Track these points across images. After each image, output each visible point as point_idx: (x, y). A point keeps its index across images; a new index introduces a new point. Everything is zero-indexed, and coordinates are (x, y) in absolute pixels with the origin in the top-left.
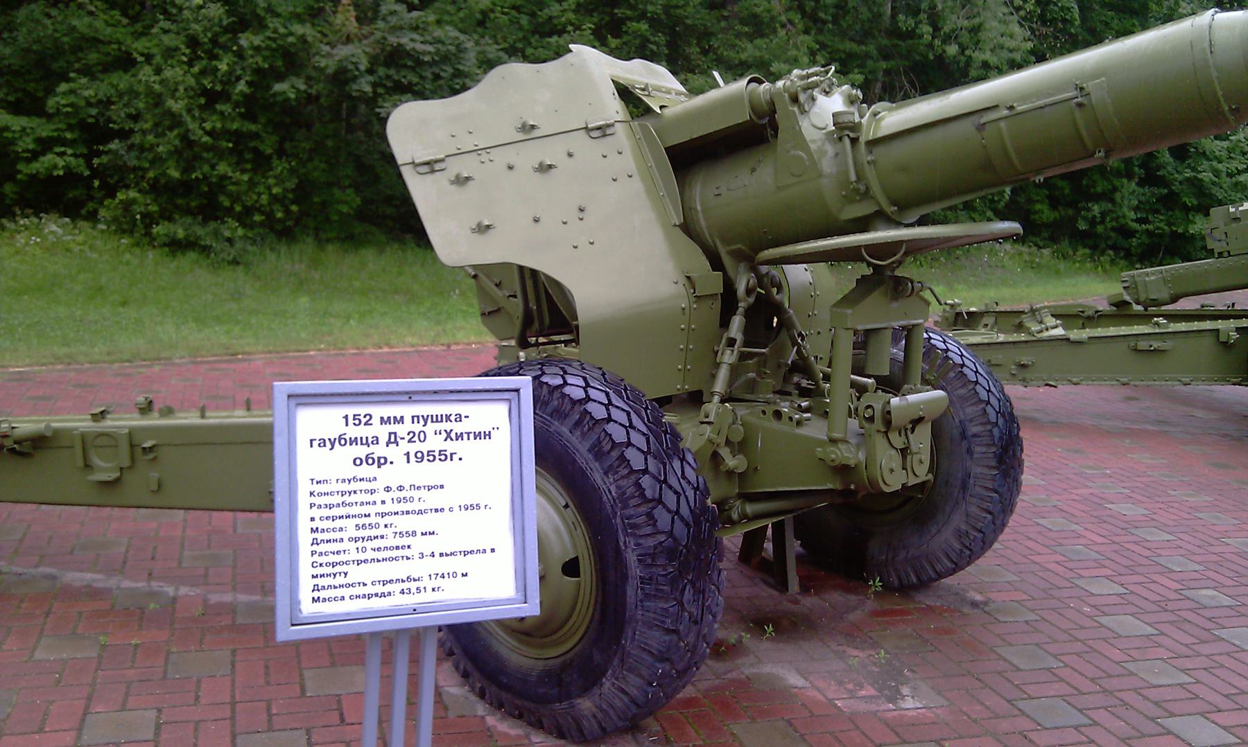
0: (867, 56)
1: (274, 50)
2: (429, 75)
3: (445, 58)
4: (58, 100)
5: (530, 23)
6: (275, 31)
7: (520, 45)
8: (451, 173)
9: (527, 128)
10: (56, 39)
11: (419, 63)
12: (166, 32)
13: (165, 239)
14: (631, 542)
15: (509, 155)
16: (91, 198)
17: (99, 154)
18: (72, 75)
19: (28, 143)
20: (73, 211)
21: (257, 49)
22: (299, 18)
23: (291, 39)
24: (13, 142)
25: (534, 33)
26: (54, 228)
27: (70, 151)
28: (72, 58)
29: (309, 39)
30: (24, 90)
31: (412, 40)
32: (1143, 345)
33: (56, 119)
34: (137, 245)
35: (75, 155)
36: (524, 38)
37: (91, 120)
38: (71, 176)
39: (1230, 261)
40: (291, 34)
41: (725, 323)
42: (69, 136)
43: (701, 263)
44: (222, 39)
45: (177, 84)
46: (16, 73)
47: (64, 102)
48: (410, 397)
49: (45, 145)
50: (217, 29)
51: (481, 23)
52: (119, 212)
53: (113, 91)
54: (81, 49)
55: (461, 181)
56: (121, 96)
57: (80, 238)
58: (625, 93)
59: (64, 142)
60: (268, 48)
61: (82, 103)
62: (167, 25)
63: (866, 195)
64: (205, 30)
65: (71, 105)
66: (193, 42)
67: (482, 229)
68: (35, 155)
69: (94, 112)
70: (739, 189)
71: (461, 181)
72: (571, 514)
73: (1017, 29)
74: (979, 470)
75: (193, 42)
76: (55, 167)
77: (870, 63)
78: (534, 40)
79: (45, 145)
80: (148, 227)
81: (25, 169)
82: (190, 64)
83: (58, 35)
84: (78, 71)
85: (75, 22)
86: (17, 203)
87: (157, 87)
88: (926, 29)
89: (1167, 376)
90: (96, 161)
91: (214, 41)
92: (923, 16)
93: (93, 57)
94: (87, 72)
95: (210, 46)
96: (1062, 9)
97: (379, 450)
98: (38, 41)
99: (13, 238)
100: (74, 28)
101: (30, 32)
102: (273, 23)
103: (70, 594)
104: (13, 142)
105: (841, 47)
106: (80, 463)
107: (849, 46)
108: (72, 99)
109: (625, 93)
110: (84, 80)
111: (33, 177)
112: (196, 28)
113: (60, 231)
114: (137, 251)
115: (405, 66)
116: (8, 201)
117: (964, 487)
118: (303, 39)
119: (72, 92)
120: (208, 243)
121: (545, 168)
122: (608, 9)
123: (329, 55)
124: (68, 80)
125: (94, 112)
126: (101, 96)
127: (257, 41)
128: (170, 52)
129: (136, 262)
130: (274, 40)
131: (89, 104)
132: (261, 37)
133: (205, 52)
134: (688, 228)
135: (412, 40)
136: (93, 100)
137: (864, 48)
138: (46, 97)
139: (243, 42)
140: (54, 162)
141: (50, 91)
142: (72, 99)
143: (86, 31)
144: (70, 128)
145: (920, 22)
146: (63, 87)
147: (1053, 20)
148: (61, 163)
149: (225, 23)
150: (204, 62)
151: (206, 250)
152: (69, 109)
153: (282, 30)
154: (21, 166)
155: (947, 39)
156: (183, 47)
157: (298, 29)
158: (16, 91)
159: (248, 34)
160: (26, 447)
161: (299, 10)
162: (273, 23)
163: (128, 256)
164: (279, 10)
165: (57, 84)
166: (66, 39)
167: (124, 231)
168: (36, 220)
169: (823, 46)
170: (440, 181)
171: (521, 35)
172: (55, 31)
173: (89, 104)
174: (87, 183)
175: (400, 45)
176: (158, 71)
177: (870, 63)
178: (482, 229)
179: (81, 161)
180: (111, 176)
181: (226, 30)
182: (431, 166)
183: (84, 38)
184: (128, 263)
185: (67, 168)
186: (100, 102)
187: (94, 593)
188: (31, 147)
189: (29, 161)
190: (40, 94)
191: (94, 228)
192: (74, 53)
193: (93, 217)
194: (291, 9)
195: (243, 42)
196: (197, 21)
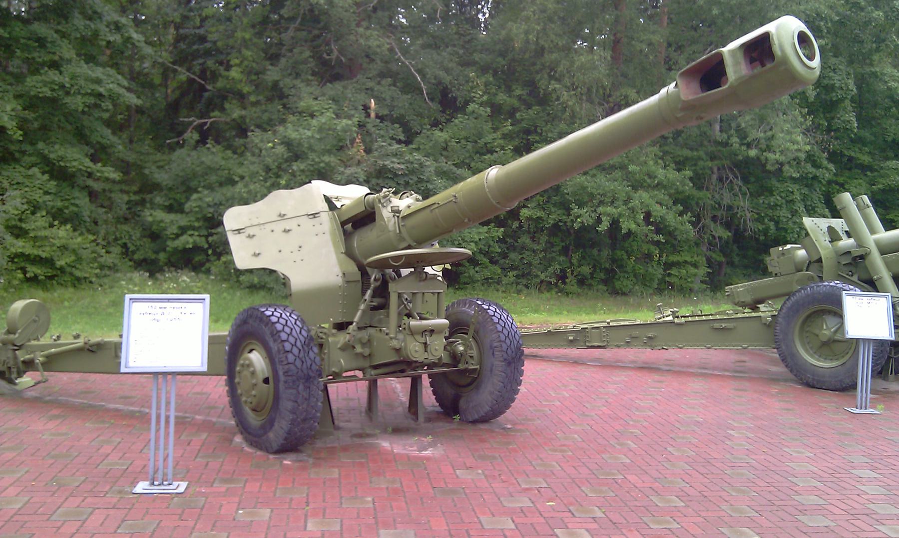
0: (700, 158)
1: (312, 171)
2: (402, 182)
3: (412, 172)
4: (191, 204)
5: (473, 147)
6: (313, 160)
7: (467, 161)
8: (246, 234)
9: (282, 216)
10: (193, 169)
11: (396, 175)
12: (253, 163)
13: (248, 284)
14: (281, 367)
15: (272, 226)
16: (208, 261)
17: (211, 235)
18: (200, 189)
19: (174, 229)
20: (197, 268)
21: (303, 171)
22: (329, 152)
23: (322, 165)
24: (165, 229)
25: (477, 153)
26: (185, 278)
27: (196, 233)
28: (202, 179)
29: (332, 164)
30: (174, 199)
31: (392, 162)
32: (717, 325)
33: (189, 215)
34: (232, 288)
35: (200, 236)
36: (470, 156)
37: (210, 215)
38: (197, 249)
39: (781, 279)
40: (323, 161)
41: (364, 293)
42: (196, 224)
43: (353, 268)
44: (284, 166)
45: (256, 193)
46: (170, 189)
47: (194, 205)
48: (169, 300)
49: (183, 230)
50: (280, 160)
51: (445, 149)
52: (222, 268)
53: (223, 198)
54: (207, 174)
55: (250, 237)
56: (227, 201)
57: (199, 284)
58: (328, 200)
59: (194, 229)
60: (309, 170)
61: (205, 205)
62: (254, 159)
63: (404, 240)
64: (274, 161)
65: (199, 207)
66: (268, 169)
67: (257, 255)
68: (177, 236)
69: (211, 210)
70: (366, 237)
71: (250, 237)
72: (267, 360)
73: (799, 138)
74: (497, 363)
75: (268, 169)
76: (188, 243)
77: (701, 163)
78: (476, 157)
79: (183, 230)
80: (238, 277)
81: (171, 245)
82: (265, 180)
83: (194, 166)
84: (204, 187)
85: (204, 159)
86: (166, 264)
87: (245, 195)
88: (735, 140)
89: (734, 344)
90: (210, 239)
91: (279, 167)
92: (733, 132)
93: (213, 178)
94: (210, 187)
95: (276, 170)
96: (844, 122)
97: (157, 317)
98: (183, 170)
99: (161, 284)
100: (202, 163)
101: (179, 165)
102: (312, 156)
103: (108, 410)
104: (165, 229)
105: (680, 153)
106: (113, 354)
107: (687, 153)
108: (199, 203)
109: (328, 200)
110: (206, 192)
111: (175, 249)
112: (269, 160)
113: (188, 280)
114: (231, 291)
115: (387, 177)
116: (161, 263)
117: (491, 371)
118: (328, 164)
119: (200, 199)
120: (272, 286)
121: (286, 231)
122: (525, 136)
123: (343, 173)
124: (198, 192)
125: (211, 210)
126: (216, 201)
127: (302, 167)
128: (253, 175)
129: (229, 297)
130: (312, 165)
131: (209, 206)
132: (305, 164)
133: (274, 174)
134: (349, 253)
135: (392, 162)
136: (211, 204)
137: (695, 153)
138: (186, 202)
139: (295, 168)
140: (187, 241)
141: (188, 199)
142: (199, 203)
143: (208, 163)
144: (198, 220)
145: (732, 135)
146: (195, 196)
147: (837, 130)
148: (191, 240)
149: (285, 156)
150: (273, 180)
151: (270, 290)
152: (197, 209)
153: (317, 160)
154: (169, 243)
155: (749, 146)
156: (260, 171)
157: (326, 158)
158: (170, 199)
159: (298, 163)
160: (94, 349)
161: (328, 147)
162: (312, 156)
163: (225, 294)
164: (316, 148)
165: (191, 195)
166: (198, 169)
167: (225, 280)
168: (174, 274)
169: (665, 153)
170: (242, 236)
171: (468, 155)
172: (193, 164)
173: (209, 206)
174: (205, 251)
175: (384, 165)
176: (246, 186)
177: (701, 163)
178: (257, 255)
179: (203, 239)
180: (218, 247)
181: (286, 161)
182: (239, 231)
183: (209, 168)
184: (225, 298)
185: (195, 242)
186: (216, 204)
187: (117, 410)
188: (175, 231)
189: (174, 239)
190: (183, 201)
191: (208, 278)
192: (203, 176)
193: (208, 272)
194: (323, 147)
195: (295, 168)
196: (269, 156)
